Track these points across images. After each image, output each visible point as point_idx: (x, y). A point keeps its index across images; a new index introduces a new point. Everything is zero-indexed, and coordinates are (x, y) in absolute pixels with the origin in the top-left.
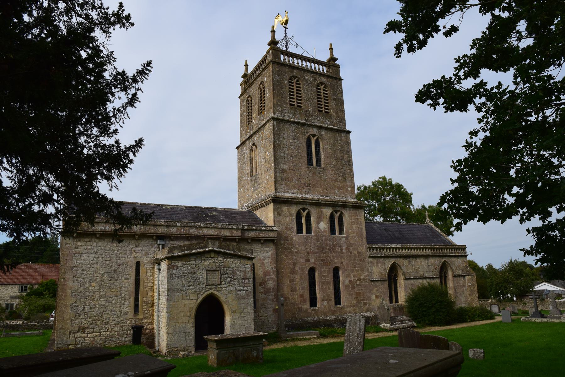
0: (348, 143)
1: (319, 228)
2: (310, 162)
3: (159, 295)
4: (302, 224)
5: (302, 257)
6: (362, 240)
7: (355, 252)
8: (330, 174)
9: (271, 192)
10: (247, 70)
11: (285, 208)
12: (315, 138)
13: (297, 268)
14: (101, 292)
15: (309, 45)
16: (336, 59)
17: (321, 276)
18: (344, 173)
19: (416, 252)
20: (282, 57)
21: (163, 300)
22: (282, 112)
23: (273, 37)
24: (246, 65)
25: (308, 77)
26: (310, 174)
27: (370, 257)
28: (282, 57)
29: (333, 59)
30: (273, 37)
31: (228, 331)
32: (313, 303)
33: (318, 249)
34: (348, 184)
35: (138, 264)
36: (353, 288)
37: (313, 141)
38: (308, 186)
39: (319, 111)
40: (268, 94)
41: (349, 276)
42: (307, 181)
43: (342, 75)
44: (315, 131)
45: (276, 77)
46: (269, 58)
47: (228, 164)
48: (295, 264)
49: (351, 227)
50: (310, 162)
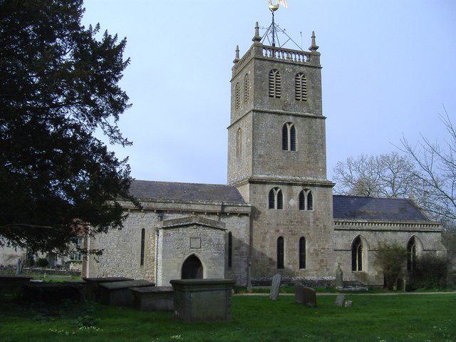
0: (323, 129)
1: (289, 204)
2: (285, 147)
3: (157, 254)
4: (275, 200)
5: (273, 228)
6: (329, 215)
7: (321, 225)
8: (303, 157)
9: (249, 174)
10: (238, 55)
11: (259, 187)
12: (291, 125)
13: (268, 237)
14: (132, 253)
15: (294, 39)
16: (317, 48)
17: (288, 241)
18: (316, 156)
19: (386, 227)
20: (264, 51)
21: (160, 257)
22: (261, 104)
23: (257, 33)
24: (238, 51)
25: (288, 69)
26: (284, 158)
27: (335, 230)
28: (264, 51)
29: (314, 48)
30: (257, 33)
31: (205, 277)
32: (302, 265)
33: (287, 222)
34: (320, 165)
35: (143, 230)
36: (317, 255)
37: (289, 128)
38: (282, 168)
39: (297, 99)
40: (251, 87)
41: (313, 245)
42: (281, 164)
43: (322, 63)
44: (291, 119)
45: (258, 72)
46: (253, 55)
47: (219, 143)
48: (266, 233)
49: (319, 204)
50: (285, 147)
